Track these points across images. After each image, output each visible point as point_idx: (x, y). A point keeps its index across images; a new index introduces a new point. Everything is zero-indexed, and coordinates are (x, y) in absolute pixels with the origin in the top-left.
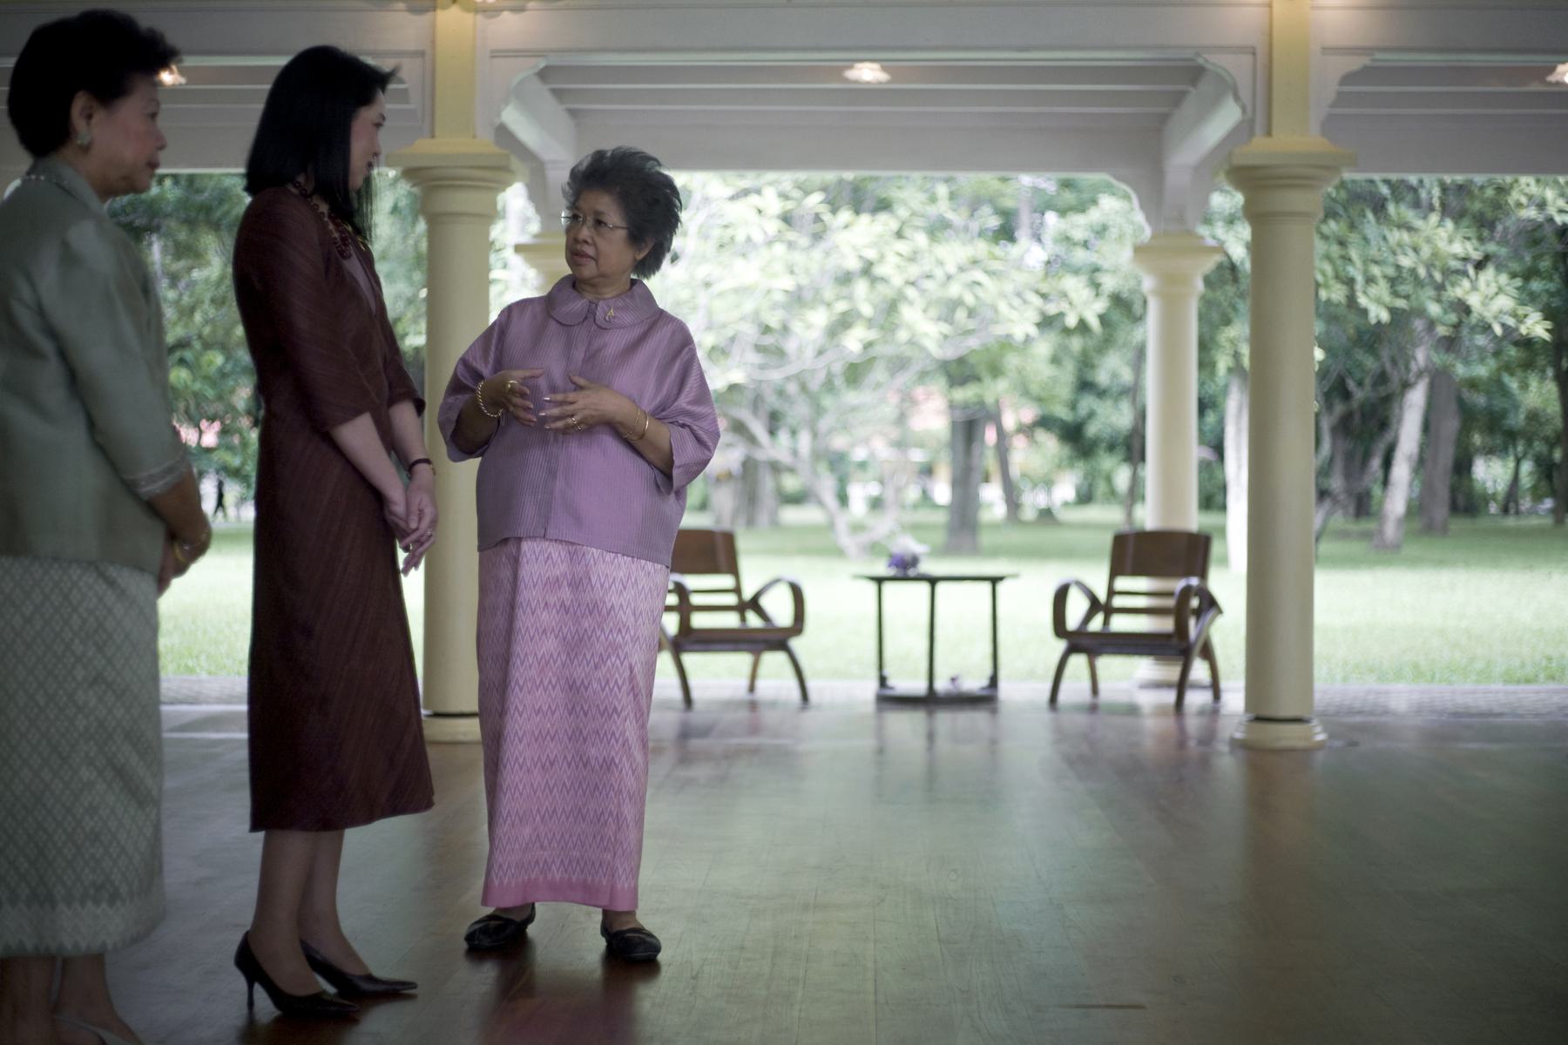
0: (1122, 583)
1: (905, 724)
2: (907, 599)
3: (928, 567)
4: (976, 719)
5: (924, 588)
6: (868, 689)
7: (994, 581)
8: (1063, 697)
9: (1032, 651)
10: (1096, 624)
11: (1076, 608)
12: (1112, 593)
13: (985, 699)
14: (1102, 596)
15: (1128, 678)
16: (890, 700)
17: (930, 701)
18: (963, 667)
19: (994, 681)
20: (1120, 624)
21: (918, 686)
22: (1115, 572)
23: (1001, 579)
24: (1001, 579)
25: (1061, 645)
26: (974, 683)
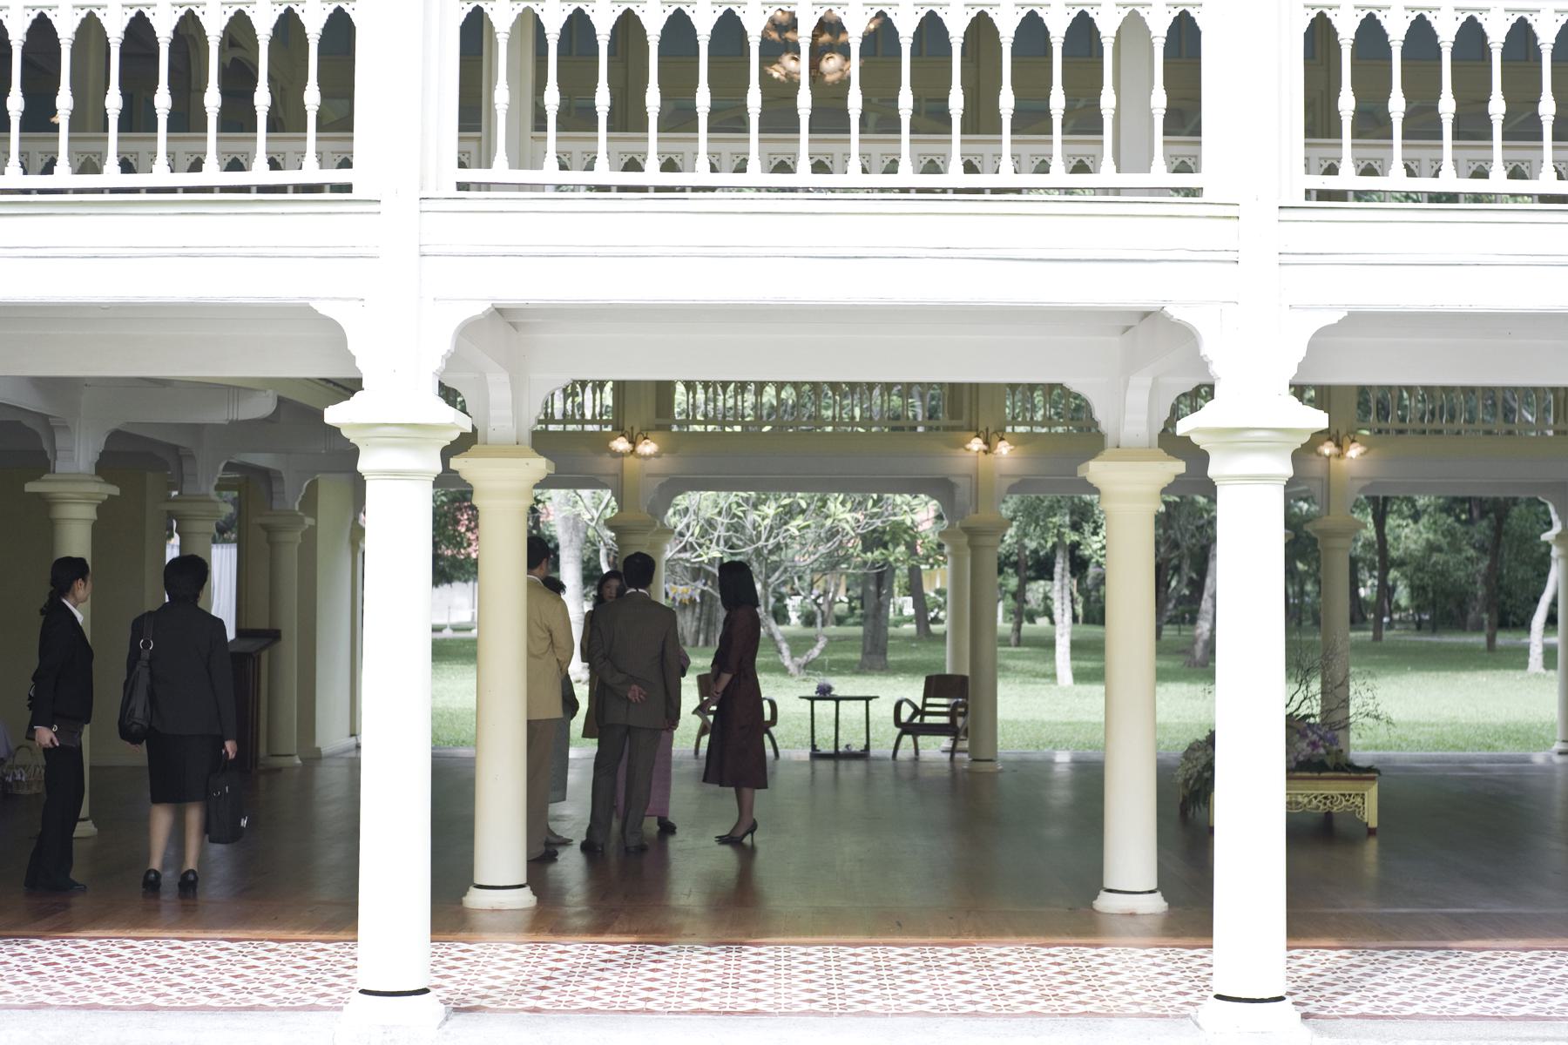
0: (929, 701)
1: (822, 765)
2: (825, 708)
3: (836, 692)
4: (857, 767)
5: (833, 703)
6: (805, 754)
7: (868, 699)
8: (900, 754)
9: (884, 736)
10: (917, 720)
11: (906, 712)
12: (925, 705)
13: (864, 755)
14: (920, 706)
15: (935, 748)
16: (816, 755)
17: (836, 756)
18: (853, 739)
19: (867, 747)
20: (928, 720)
21: (831, 750)
22: (927, 694)
23: (871, 698)
24: (871, 698)
25: (898, 730)
26: (858, 746)
